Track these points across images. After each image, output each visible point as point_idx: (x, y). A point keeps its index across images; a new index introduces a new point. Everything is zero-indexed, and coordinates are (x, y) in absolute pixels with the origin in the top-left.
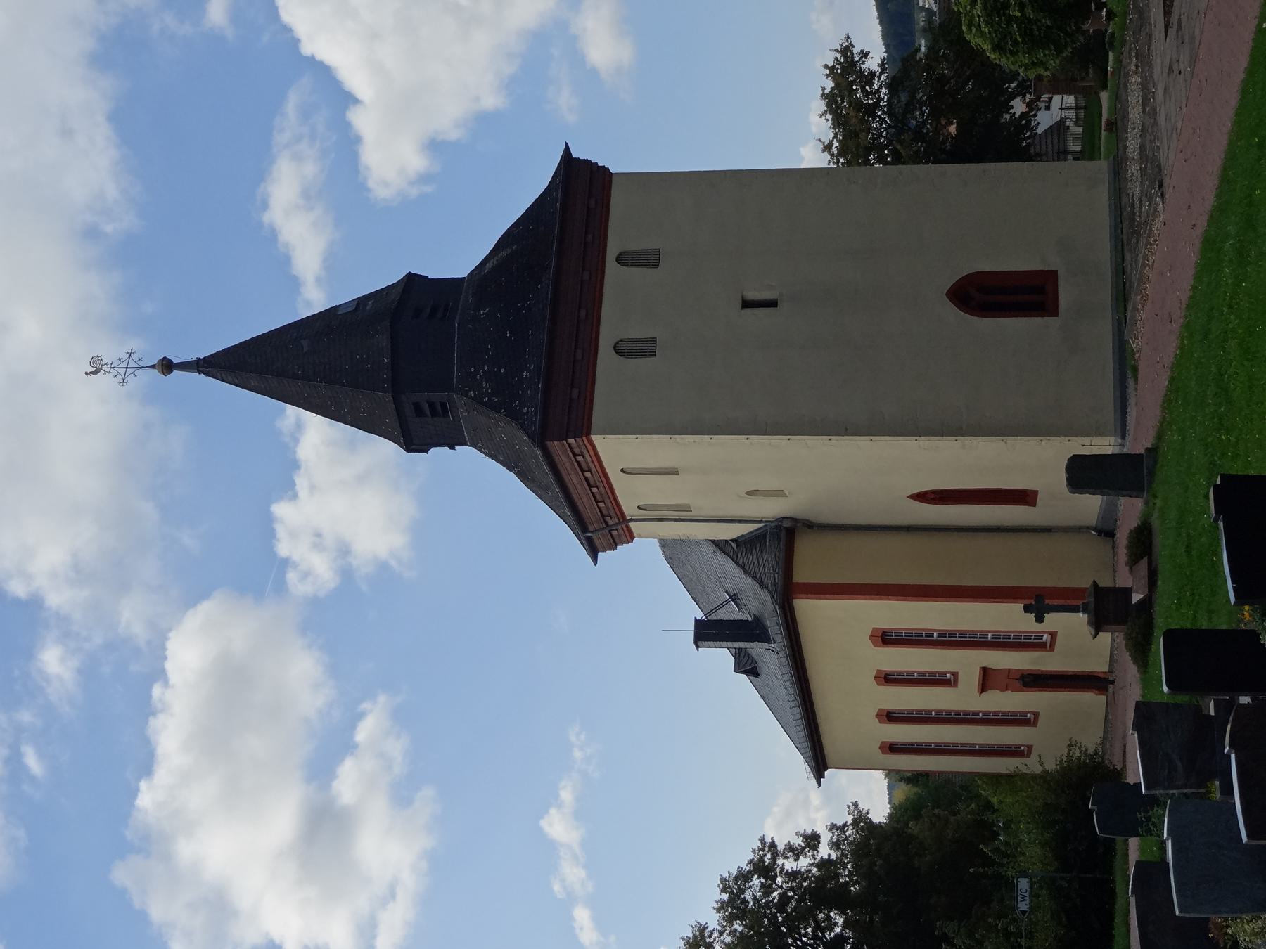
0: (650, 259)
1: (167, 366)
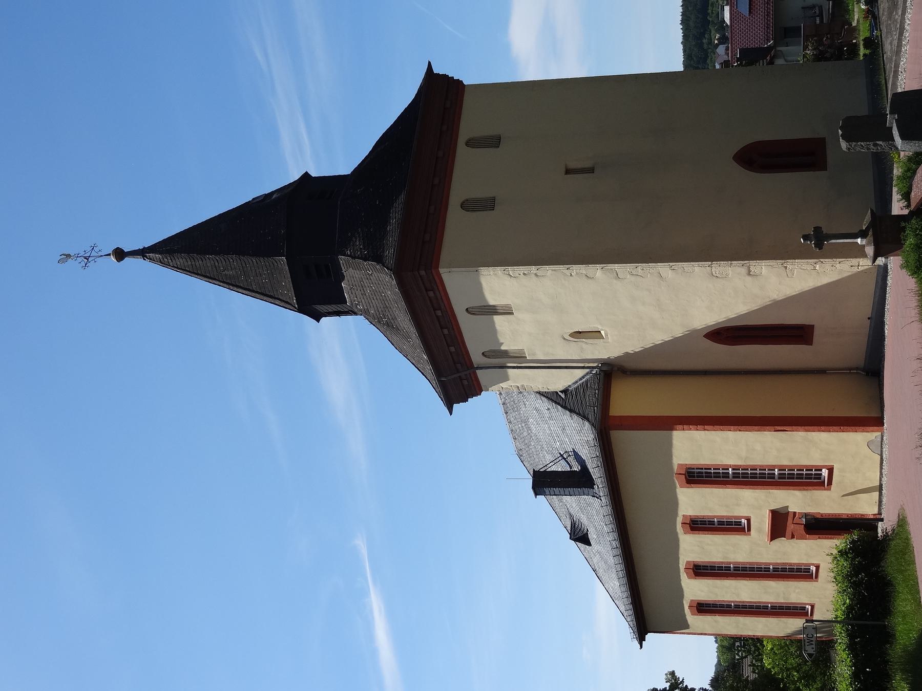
1: (120, 254)
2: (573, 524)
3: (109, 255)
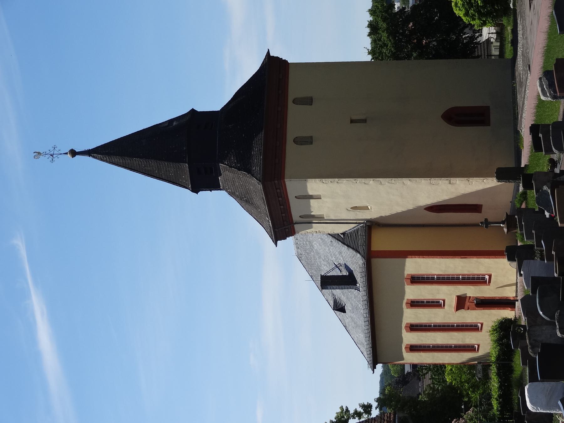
0: (308, 101)
1: (73, 153)
2: (335, 300)
3: (66, 153)
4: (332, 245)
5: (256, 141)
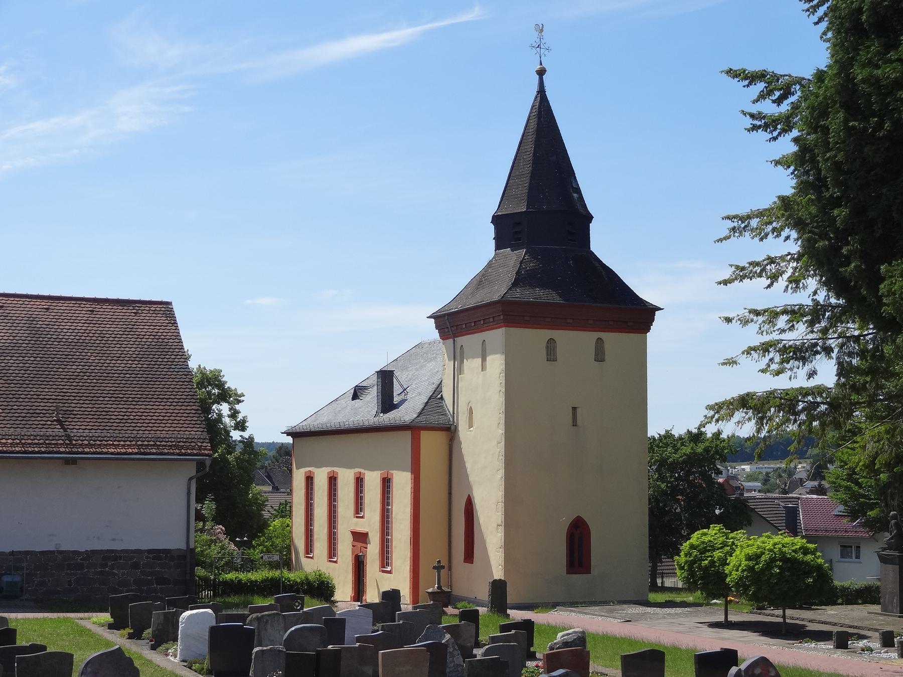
0: (600, 356)
1: (541, 73)
3: (541, 64)
4: (429, 384)
5: (552, 294)
